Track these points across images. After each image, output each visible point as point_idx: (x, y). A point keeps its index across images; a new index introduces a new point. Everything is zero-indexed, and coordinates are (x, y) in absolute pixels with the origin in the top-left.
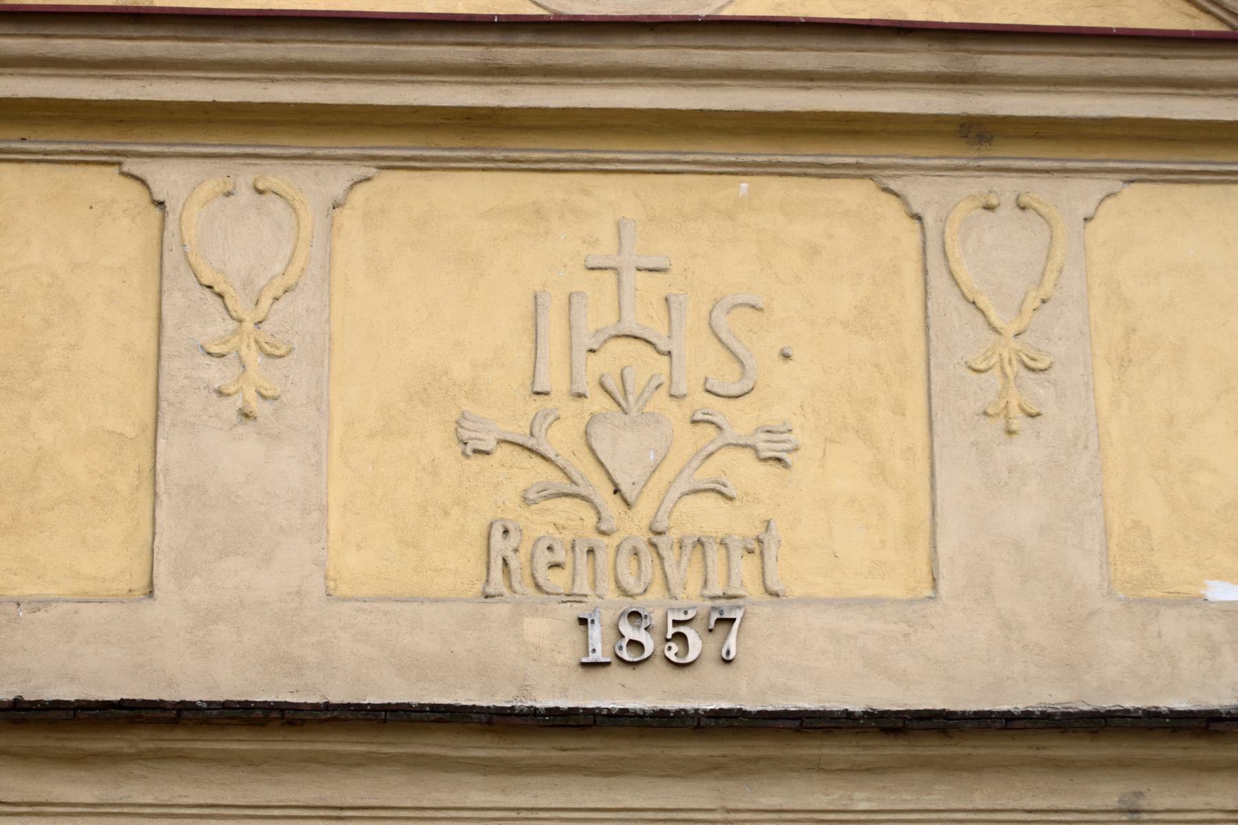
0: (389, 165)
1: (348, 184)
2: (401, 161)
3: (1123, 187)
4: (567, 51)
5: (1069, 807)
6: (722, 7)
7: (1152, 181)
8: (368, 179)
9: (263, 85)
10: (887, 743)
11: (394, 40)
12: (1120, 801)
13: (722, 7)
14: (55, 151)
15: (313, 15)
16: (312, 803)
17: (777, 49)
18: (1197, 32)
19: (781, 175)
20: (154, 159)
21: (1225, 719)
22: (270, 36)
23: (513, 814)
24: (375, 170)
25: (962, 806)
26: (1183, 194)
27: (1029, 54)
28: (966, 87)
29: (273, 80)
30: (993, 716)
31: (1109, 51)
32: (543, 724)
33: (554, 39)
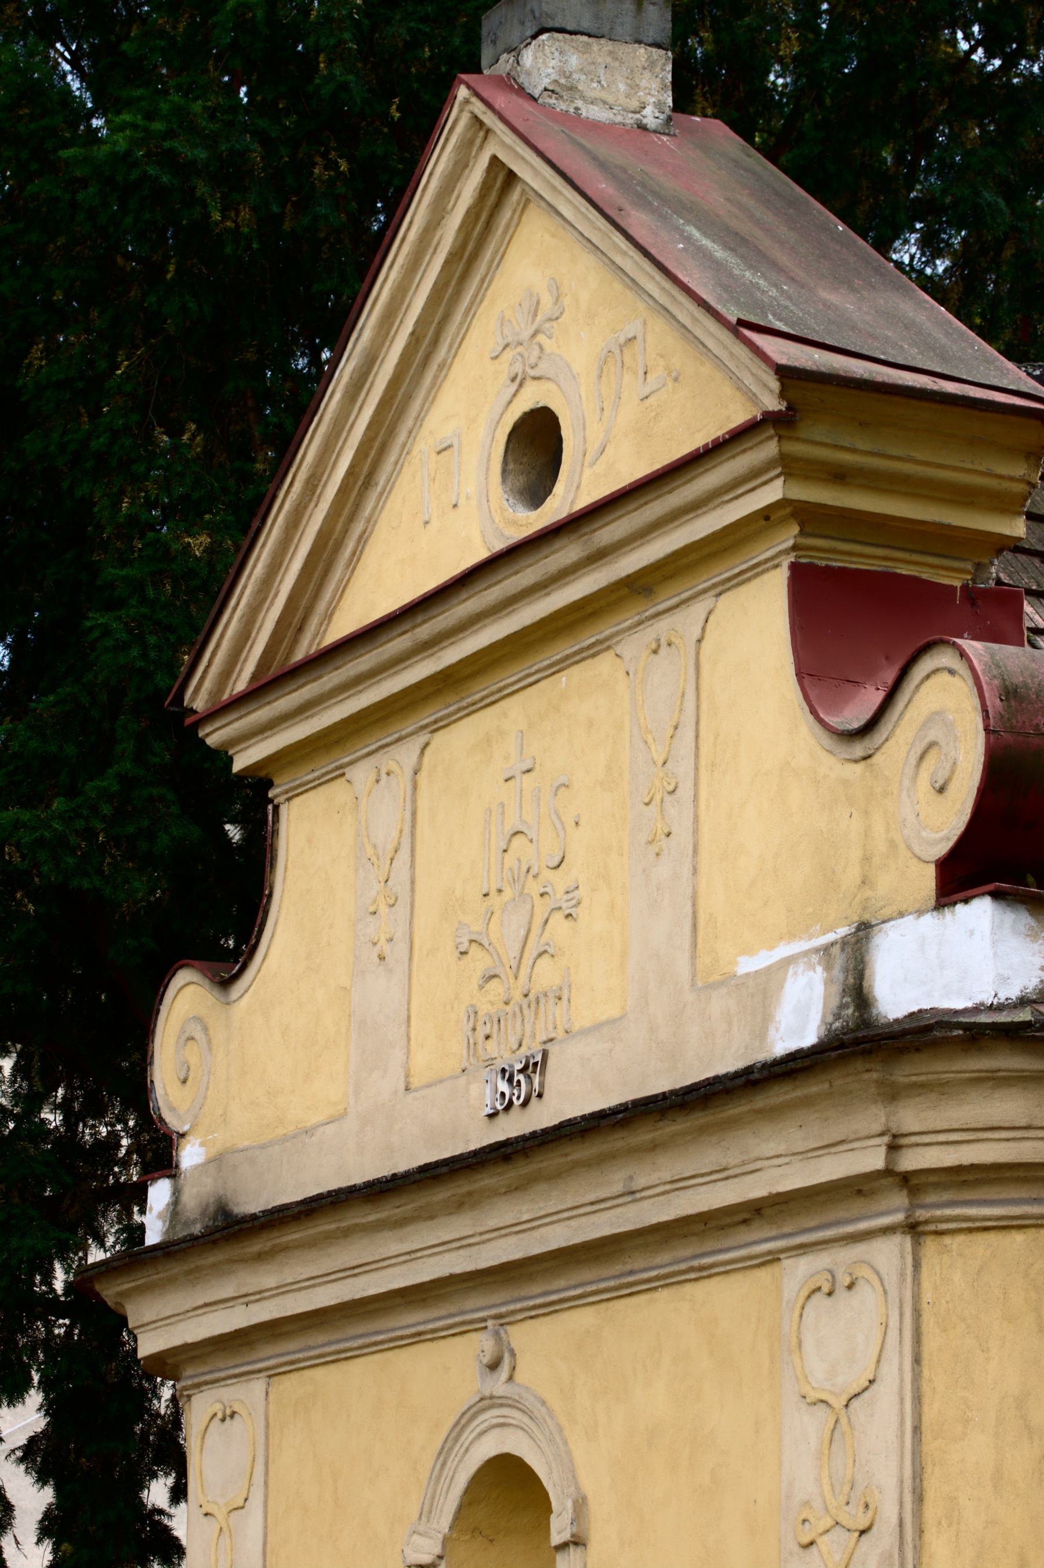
0: (437, 727)
1: (418, 752)
2: (456, 713)
3: (717, 601)
4: (441, 618)
5: (604, 1196)
6: (573, 502)
7: (729, 589)
8: (427, 744)
9: (356, 698)
10: (479, 1177)
11: (377, 644)
12: (624, 1186)
13: (573, 502)
14: (592, 648)
15: (638, 484)
16: (681, 1192)
17: (295, 690)
18: (630, 485)
19: (577, 662)
20: (355, 765)
21: (610, 1115)
22: (516, 567)
23: (407, 1257)
24: (429, 735)
25: (564, 1207)
26: (743, 589)
27: (612, 521)
28: (606, 559)
29: (360, 692)
30: (487, 1150)
31: (642, 501)
32: (155, 1253)
33: (339, 662)
